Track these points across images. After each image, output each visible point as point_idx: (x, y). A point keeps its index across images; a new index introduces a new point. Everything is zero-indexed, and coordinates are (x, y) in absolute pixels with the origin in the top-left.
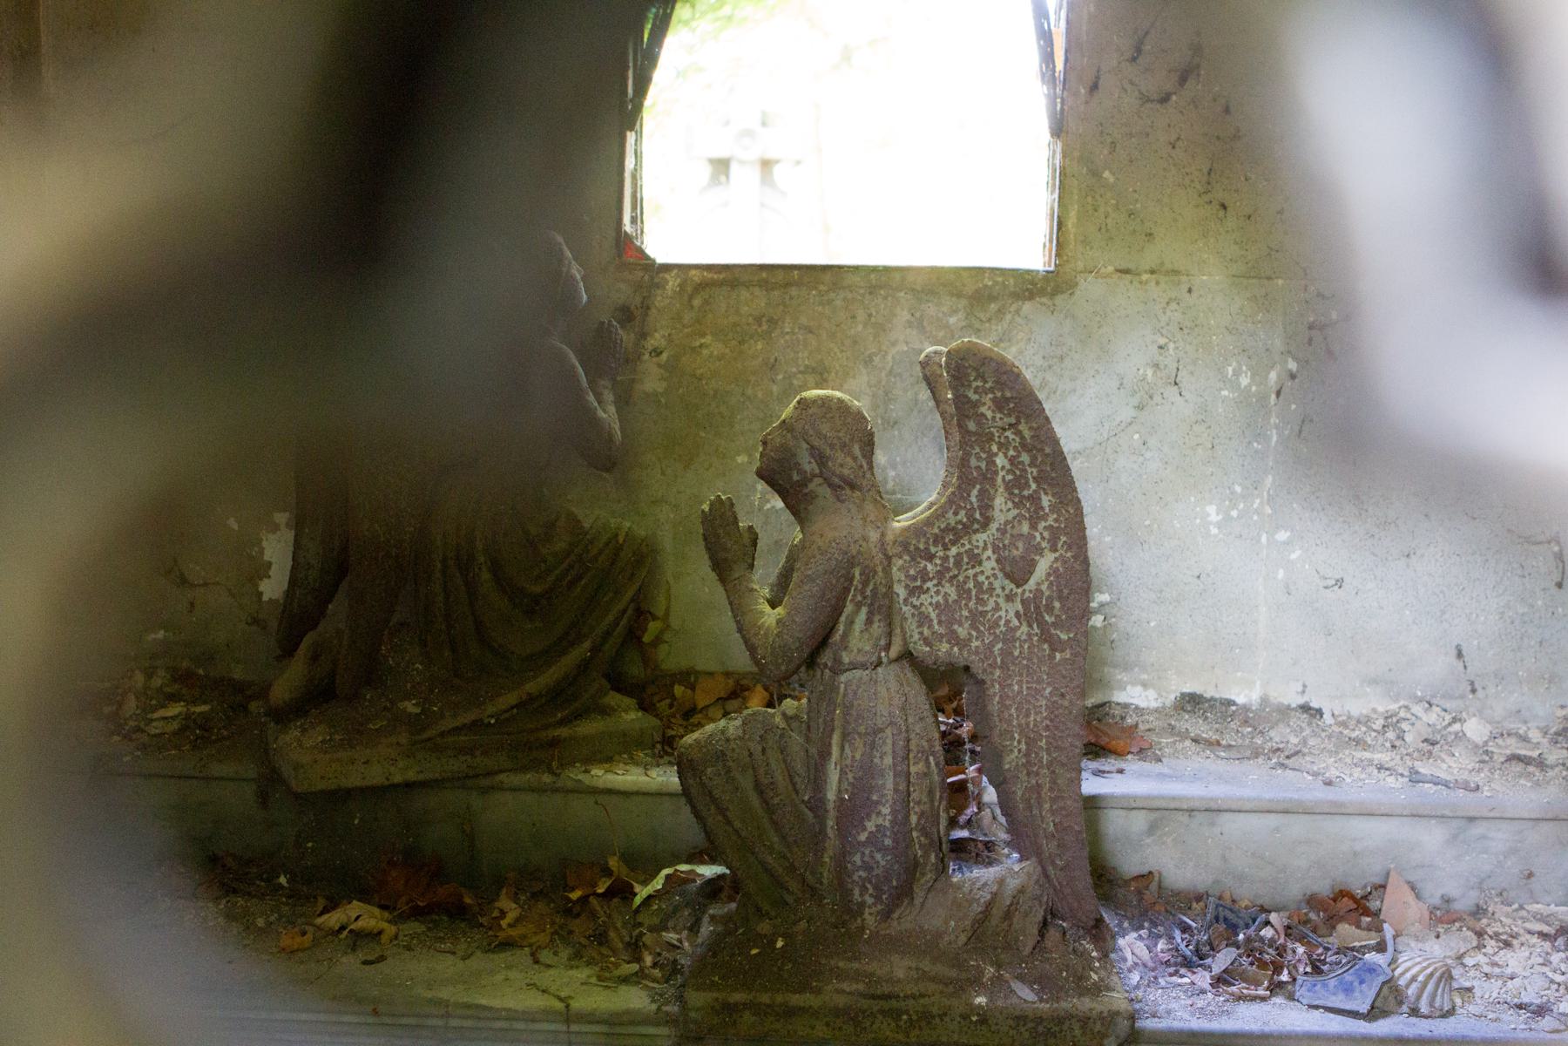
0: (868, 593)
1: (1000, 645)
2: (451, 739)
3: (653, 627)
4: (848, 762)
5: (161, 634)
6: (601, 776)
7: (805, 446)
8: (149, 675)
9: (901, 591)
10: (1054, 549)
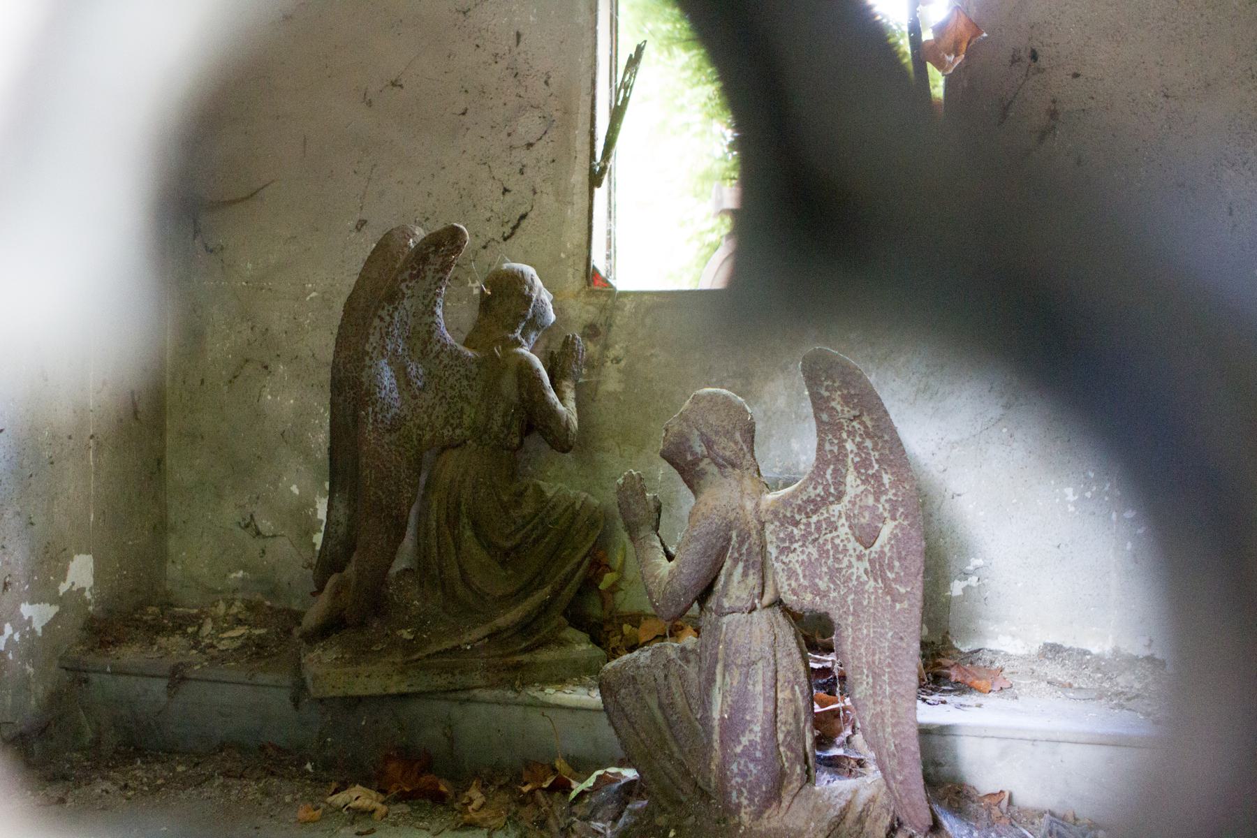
0: (744, 551)
1: (852, 596)
2: (436, 661)
3: (609, 578)
4: (728, 688)
5: (240, 574)
6: (552, 694)
7: (696, 433)
8: (230, 604)
9: (772, 550)
10: (894, 518)
